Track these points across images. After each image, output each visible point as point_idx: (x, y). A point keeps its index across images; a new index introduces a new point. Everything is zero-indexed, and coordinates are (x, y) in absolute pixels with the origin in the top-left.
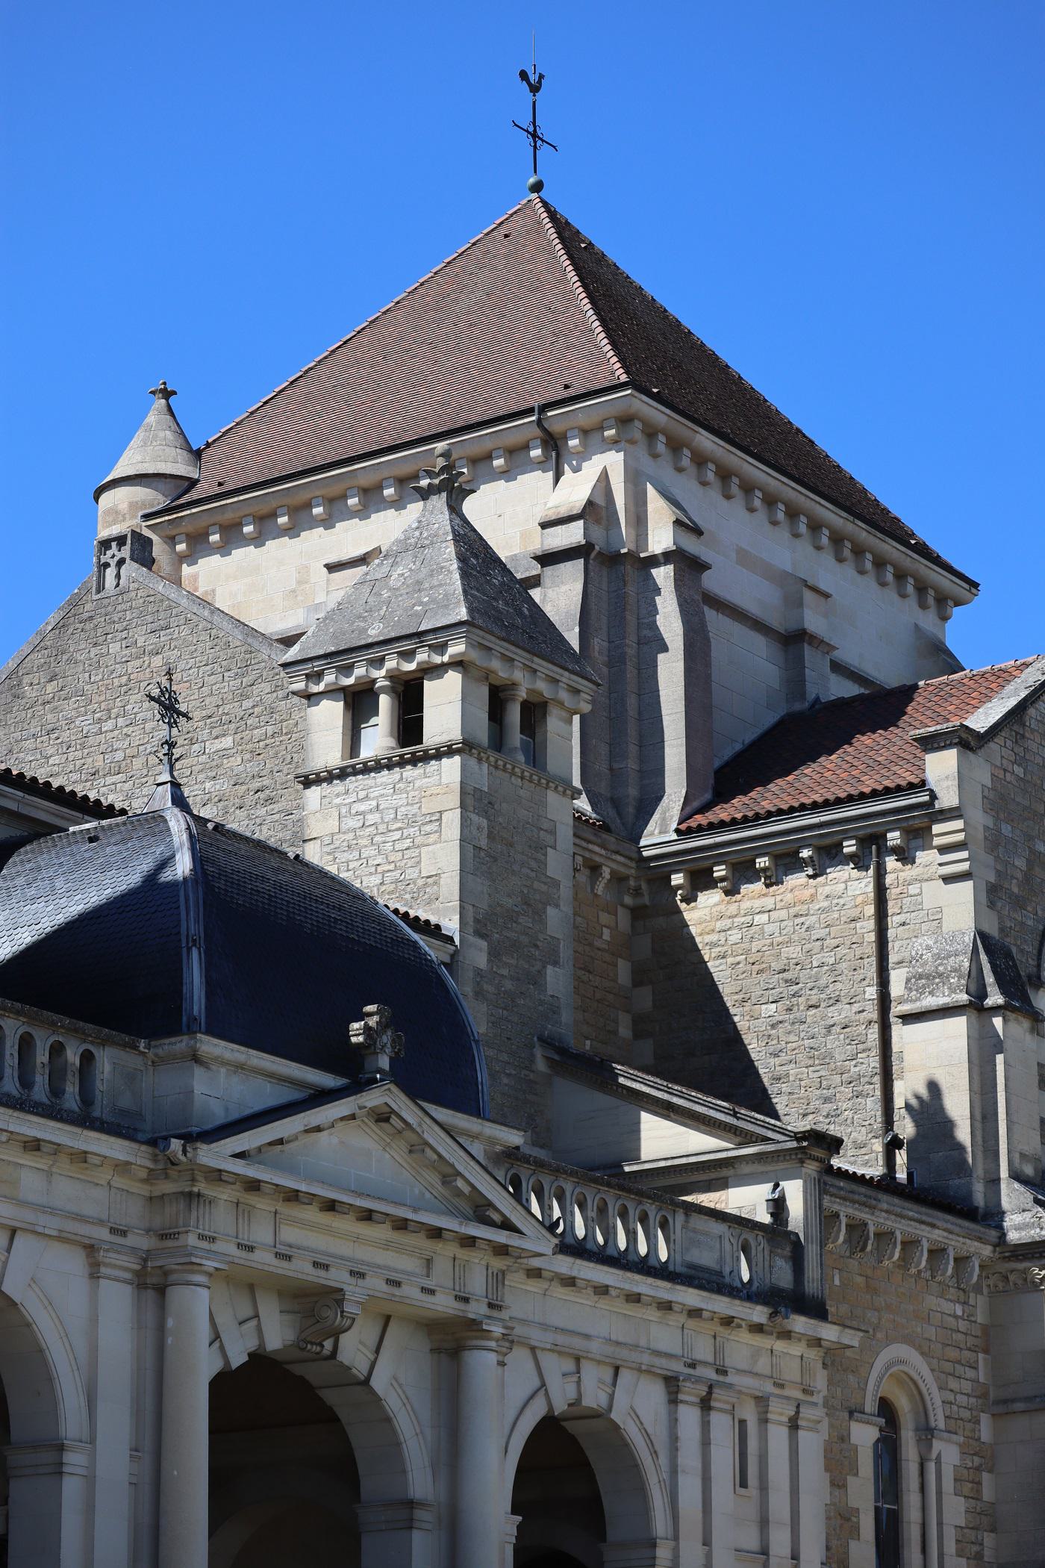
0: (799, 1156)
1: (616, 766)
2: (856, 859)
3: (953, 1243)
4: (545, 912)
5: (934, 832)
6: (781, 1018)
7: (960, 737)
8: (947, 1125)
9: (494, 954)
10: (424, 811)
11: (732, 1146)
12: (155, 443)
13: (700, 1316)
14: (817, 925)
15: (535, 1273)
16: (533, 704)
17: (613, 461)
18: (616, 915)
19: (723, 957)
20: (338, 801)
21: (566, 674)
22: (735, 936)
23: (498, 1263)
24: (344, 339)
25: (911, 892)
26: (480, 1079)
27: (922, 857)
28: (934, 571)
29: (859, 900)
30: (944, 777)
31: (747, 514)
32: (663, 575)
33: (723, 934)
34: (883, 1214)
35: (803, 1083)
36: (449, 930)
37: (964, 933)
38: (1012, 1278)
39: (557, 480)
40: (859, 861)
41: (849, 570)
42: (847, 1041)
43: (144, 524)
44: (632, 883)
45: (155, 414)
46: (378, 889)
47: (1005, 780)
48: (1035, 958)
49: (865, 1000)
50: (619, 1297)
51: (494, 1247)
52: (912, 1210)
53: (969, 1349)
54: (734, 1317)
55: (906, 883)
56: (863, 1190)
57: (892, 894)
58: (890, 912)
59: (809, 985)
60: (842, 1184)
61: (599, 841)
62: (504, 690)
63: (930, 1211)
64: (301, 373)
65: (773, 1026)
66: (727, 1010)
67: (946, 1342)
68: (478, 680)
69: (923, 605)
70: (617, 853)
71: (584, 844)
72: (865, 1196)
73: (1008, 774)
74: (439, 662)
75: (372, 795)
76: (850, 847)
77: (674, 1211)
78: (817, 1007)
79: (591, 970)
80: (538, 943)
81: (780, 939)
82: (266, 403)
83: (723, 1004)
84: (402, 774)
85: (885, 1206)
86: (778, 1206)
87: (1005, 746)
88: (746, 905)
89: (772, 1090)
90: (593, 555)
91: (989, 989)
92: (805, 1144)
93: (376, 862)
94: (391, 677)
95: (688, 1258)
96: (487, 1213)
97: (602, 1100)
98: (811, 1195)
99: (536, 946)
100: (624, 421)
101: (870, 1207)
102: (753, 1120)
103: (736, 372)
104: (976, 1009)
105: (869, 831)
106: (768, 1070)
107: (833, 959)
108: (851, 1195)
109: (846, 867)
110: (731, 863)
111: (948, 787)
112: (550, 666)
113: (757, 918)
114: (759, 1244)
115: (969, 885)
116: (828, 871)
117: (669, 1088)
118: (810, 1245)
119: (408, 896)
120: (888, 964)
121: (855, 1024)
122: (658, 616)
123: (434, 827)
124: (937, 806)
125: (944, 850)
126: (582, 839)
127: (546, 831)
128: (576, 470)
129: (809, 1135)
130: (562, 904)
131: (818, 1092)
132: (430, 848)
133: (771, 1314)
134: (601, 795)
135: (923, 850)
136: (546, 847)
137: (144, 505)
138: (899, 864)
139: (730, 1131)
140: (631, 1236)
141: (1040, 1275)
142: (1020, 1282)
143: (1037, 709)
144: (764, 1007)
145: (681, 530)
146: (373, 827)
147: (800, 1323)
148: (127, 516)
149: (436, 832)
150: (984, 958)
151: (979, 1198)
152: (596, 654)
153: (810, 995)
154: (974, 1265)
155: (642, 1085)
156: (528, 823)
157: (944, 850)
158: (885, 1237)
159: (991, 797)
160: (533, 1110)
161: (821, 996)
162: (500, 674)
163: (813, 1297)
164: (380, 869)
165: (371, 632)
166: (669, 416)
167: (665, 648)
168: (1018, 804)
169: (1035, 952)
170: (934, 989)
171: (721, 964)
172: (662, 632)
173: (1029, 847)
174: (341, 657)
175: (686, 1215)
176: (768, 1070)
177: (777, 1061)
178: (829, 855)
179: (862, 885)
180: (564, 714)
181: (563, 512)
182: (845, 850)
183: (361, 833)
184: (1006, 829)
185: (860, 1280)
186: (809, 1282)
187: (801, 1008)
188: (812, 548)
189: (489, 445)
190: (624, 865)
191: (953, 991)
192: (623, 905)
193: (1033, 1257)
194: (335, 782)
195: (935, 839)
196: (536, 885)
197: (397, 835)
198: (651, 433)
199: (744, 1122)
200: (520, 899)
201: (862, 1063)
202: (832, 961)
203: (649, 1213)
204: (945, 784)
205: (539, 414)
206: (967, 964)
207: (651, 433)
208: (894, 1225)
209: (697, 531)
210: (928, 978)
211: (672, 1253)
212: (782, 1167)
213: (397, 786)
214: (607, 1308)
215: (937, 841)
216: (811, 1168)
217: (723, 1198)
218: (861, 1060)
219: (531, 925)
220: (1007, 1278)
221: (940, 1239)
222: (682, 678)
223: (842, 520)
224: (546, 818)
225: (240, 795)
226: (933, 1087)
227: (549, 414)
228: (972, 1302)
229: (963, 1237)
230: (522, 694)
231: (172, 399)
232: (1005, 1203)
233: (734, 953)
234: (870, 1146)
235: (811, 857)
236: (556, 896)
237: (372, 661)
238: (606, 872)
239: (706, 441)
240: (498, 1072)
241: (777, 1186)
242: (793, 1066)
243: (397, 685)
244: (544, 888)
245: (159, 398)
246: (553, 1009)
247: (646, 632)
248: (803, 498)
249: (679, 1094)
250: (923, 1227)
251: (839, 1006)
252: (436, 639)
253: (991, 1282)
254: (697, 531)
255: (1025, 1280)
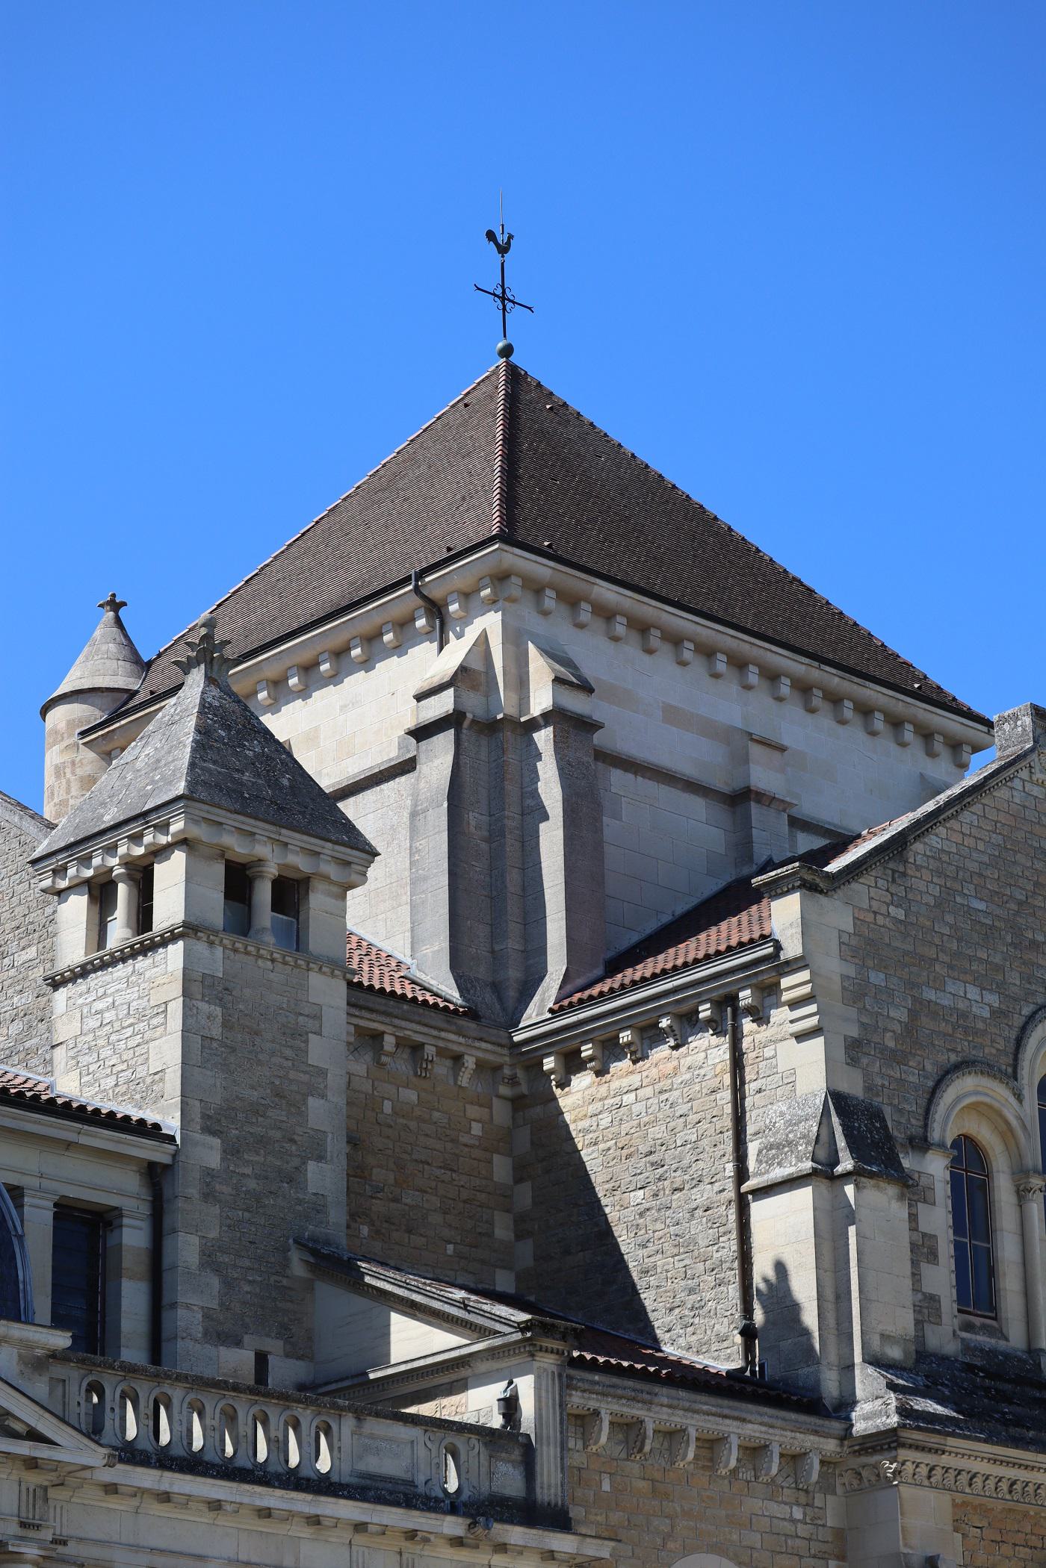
0: (527, 1349)
1: (497, 948)
2: (714, 1024)
3: (777, 1438)
4: (305, 1104)
5: (783, 986)
6: (647, 1205)
7: (802, 879)
8: (795, 1308)
9: (231, 1151)
10: (153, 1003)
11: (469, 1342)
12: (96, 658)
13: (366, 1530)
14: (680, 1101)
15: (111, 1489)
16: (297, 881)
17: (491, 623)
18: (490, 1107)
19: (595, 1144)
20: (80, 1001)
21: (329, 845)
22: (605, 1120)
23: (34, 1479)
24: (302, 531)
25: (767, 1055)
26: (21, 1278)
27: (780, 1015)
28: (936, 714)
29: (718, 1069)
30: (787, 925)
31: (678, 670)
32: (544, 738)
33: (594, 1119)
34: (665, 1409)
35: (669, 1275)
36: (170, 1128)
37: (816, 1095)
38: (864, 1473)
39: (441, 648)
40: (715, 1025)
41: (825, 720)
42: (709, 1225)
43: (81, 742)
44: (507, 1071)
45: (103, 628)
46: (113, 1091)
47: (875, 924)
48: (921, 1118)
49: (725, 1178)
50: (635, 1525)
51: (24, 1461)
52: (706, 1402)
53: (814, 1557)
54: (417, 1531)
55: (762, 1045)
56: (630, 1383)
57: (749, 1058)
58: (748, 1078)
59: (674, 1167)
60: (597, 1378)
61: (454, 1028)
62: (250, 868)
63: (736, 1404)
64: (257, 571)
65: (641, 1215)
66: (599, 1201)
67: (778, 1549)
68: (210, 858)
69: (931, 754)
70: (481, 1039)
71: (435, 1033)
72: (634, 1390)
73: (879, 917)
74: (165, 842)
75: (109, 992)
76: (705, 1011)
77: (340, 1415)
78: (681, 1190)
79: (456, 1169)
80: (296, 1137)
81: (646, 1119)
82: (219, 605)
83: (595, 1195)
84: (134, 967)
85: (665, 1401)
86: (510, 1406)
87: (876, 887)
88: (615, 1085)
89: (640, 1284)
90: (466, 724)
91: (841, 1155)
92: (529, 1334)
93: (111, 1063)
94: (126, 864)
95: (362, 1467)
96: (6, 1423)
97: (359, 1302)
98: (547, 1391)
99: (292, 1141)
100: (501, 578)
101: (644, 1402)
102: (481, 1313)
103: (726, 524)
104: (827, 1178)
105: (721, 992)
106: (636, 1263)
107: (695, 1135)
108: (612, 1390)
109: (706, 1034)
110: (600, 1041)
111: (792, 936)
112: (305, 838)
113: (625, 1097)
114: (474, 1450)
115: (819, 1042)
116: (690, 1040)
117: (408, 1284)
118: (545, 1448)
119: (138, 1096)
120: (746, 1137)
121: (716, 1205)
122: (539, 783)
123: (159, 1019)
124: (782, 958)
125: (794, 1004)
126: (431, 1027)
127: (307, 1016)
128: (459, 636)
129: (532, 1324)
130: (329, 1094)
131: (683, 1283)
132: (157, 1042)
133: (469, 1525)
134: (477, 979)
135: (777, 1008)
136: (307, 1033)
137: (81, 722)
138: (755, 1025)
139: (465, 1326)
140: (278, 1446)
141: (891, 1468)
142: (873, 1478)
143: (925, 844)
144: (632, 1194)
145: (562, 689)
146: (109, 1026)
147: (516, 1534)
148: (65, 735)
149: (162, 1024)
150: (835, 1120)
151: (830, 1386)
152: (472, 829)
153: (675, 1177)
154: (812, 1463)
155: (385, 1283)
156: (282, 1009)
157: (794, 1004)
158: (673, 1436)
159: (853, 942)
160: (286, 1319)
161: (686, 1177)
162: (237, 850)
163: (549, 1504)
164: (115, 1070)
165: (106, 818)
166: (554, 568)
167: (545, 817)
168: (896, 949)
169: (921, 1111)
170: (782, 1159)
171: (593, 1152)
172: (544, 800)
173: (911, 996)
174: (78, 847)
175: (358, 1419)
176: (636, 1263)
177: (646, 1252)
178: (688, 1023)
179: (721, 1052)
180: (335, 889)
181: (436, 681)
182: (701, 1016)
183: (99, 1033)
184: (877, 978)
185: (642, 1485)
186: (542, 1488)
187: (667, 1192)
188: (771, 699)
189: (378, 619)
190: (494, 1053)
191: (799, 1159)
192: (498, 1096)
193: (882, 1449)
194: (79, 981)
195: (784, 993)
196: (292, 1075)
197: (129, 1031)
198: (536, 589)
199: (474, 1315)
200: (269, 1091)
201: (723, 1247)
202: (694, 1138)
203: (301, 1420)
204: (790, 932)
205: (417, 581)
206: (815, 1129)
207: (536, 589)
208: (684, 1421)
209: (585, 687)
210: (778, 1148)
211: (337, 1462)
212: (516, 1362)
213: (130, 980)
214: (234, 1525)
215: (786, 996)
216: (548, 1362)
217: (463, 1401)
218: (722, 1245)
219: (285, 1119)
220: (860, 1474)
221: (757, 1435)
222: (562, 847)
223: (803, 667)
224: (308, 1002)
225: (42, 1007)
226: (780, 1268)
227: (427, 579)
228: (818, 1503)
229: (792, 1431)
230: (272, 870)
231: (122, 612)
232: (859, 1393)
233: (605, 1139)
234: (731, 1338)
235: (670, 1027)
236: (322, 1086)
237: (109, 848)
238: (470, 1062)
239: (607, 593)
240: (237, 1279)
241: (511, 1383)
242: (660, 1256)
243: (133, 872)
244: (305, 1078)
245: (107, 611)
246: (318, 1207)
247: (529, 802)
248: (747, 647)
249: (417, 1289)
250: (728, 1421)
251: (701, 1187)
252: (159, 818)
253: (846, 1480)
254: (585, 687)
255: (878, 1475)
